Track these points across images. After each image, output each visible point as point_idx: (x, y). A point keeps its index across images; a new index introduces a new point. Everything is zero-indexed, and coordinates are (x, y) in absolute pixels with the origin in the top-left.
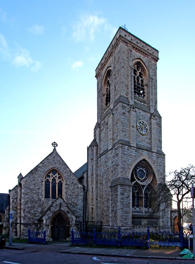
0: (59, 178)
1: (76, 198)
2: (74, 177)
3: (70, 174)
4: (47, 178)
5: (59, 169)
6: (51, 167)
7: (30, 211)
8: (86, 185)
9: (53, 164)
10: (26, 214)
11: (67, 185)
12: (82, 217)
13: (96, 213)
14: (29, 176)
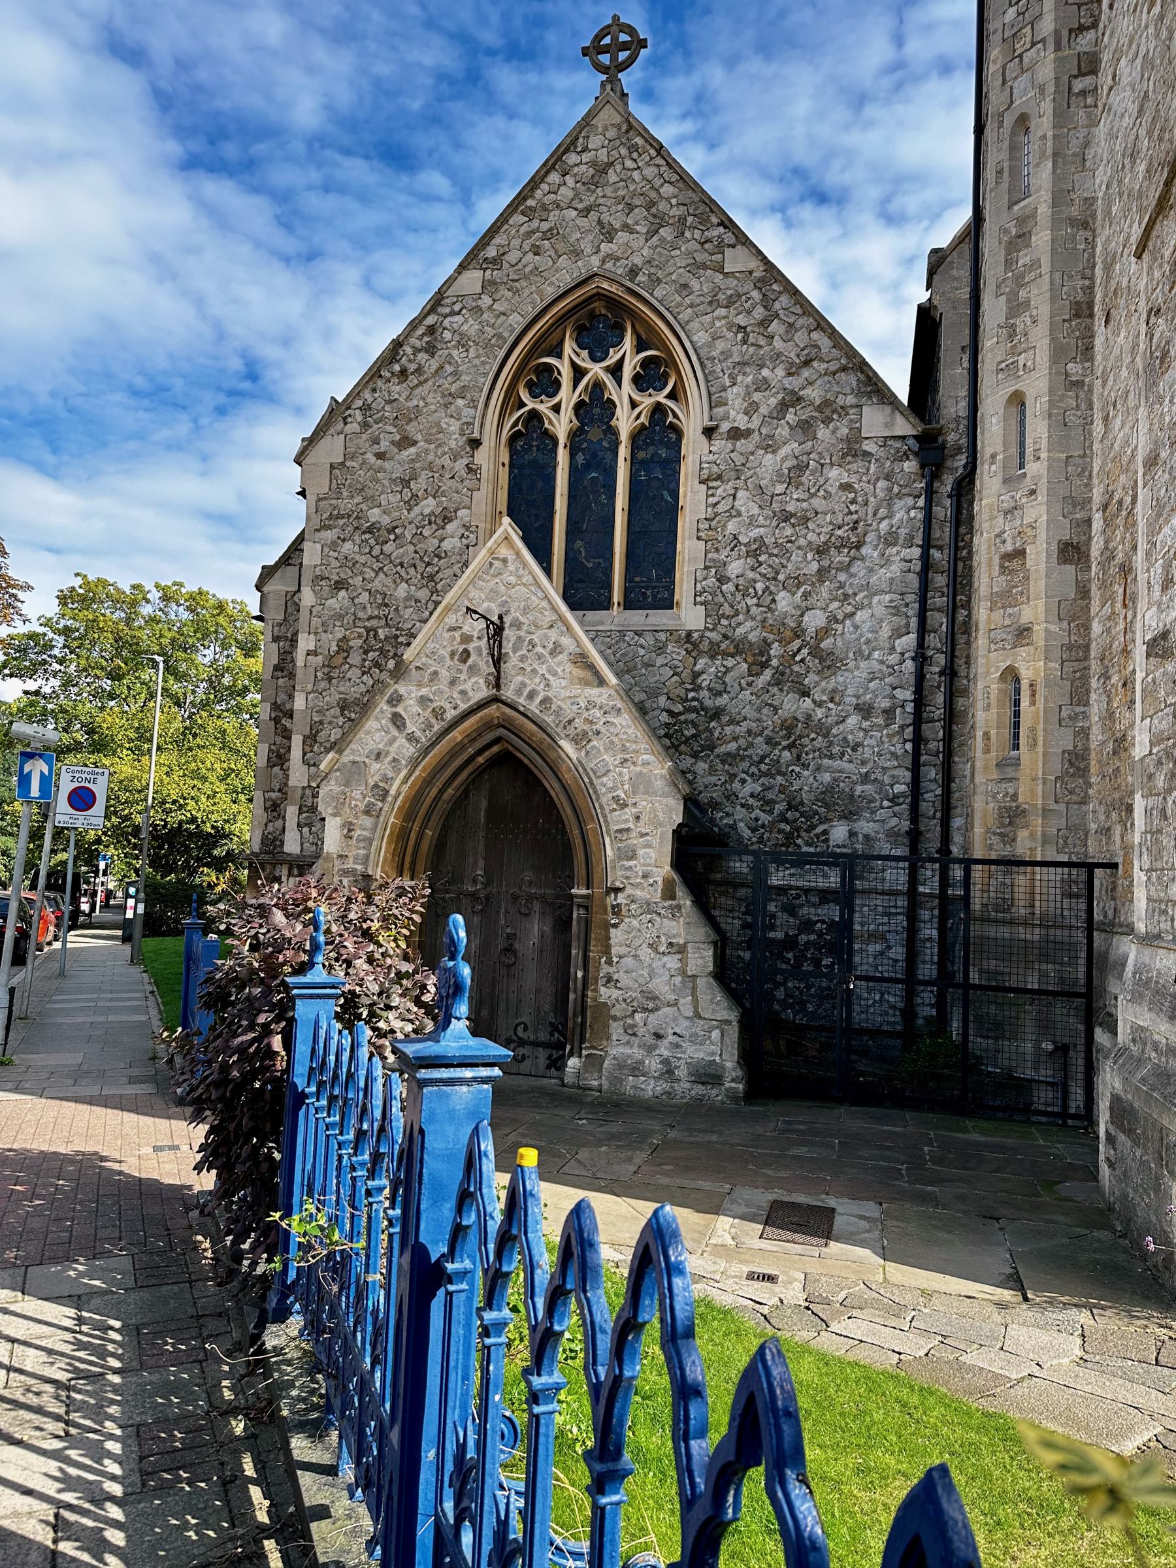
1: (822, 573)
2: (801, 337)
3: (759, 313)
4: (530, 404)
5: (641, 278)
9: (587, 247)
11: (718, 444)
12: (894, 800)
13: (1066, 741)
14: (366, 408)
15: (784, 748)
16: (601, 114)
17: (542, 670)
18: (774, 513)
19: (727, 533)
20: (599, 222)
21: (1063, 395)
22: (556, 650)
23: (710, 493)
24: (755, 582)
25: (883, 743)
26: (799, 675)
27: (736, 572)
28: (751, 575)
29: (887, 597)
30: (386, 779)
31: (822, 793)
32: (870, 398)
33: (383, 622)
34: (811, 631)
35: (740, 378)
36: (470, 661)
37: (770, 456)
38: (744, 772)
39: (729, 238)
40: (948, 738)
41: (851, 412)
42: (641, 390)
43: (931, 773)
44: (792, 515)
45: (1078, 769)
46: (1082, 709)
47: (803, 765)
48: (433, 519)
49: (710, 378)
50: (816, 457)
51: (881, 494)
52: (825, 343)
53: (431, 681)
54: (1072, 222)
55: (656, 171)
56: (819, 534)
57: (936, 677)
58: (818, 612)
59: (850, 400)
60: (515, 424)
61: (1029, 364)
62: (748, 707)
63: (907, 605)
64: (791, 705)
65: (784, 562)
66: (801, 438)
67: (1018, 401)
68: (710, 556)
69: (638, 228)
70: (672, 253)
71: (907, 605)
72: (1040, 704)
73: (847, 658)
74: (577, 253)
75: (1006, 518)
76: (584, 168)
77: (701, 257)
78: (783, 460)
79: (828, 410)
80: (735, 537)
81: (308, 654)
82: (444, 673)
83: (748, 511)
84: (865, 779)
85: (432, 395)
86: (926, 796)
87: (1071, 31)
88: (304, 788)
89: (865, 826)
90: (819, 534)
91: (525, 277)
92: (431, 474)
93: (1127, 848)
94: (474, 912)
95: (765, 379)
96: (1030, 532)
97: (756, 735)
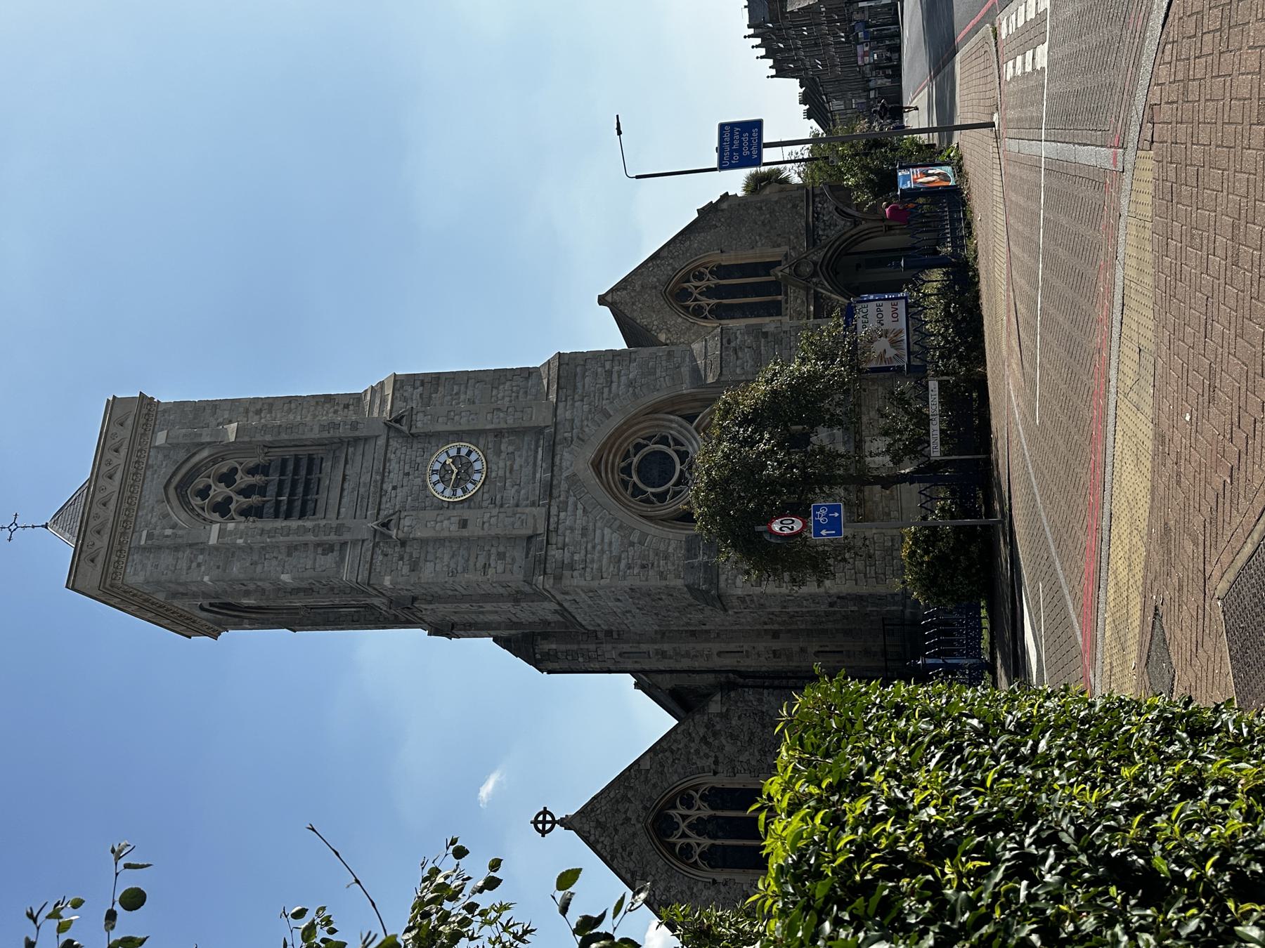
0: (700, 277)
2: (679, 737)
3: (668, 754)
6: (643, 840)
8: (710, 679)
9: (631, 830)
11: (720, 769)
37: (726, 748)
42: (693, 806)
59: (706, 717)
60: (704, 864)
67: (720, 654)
74: (634, 835)
76: (597, 833)
77: (642, 778)
78: (728, 742)
79: (710, 725)
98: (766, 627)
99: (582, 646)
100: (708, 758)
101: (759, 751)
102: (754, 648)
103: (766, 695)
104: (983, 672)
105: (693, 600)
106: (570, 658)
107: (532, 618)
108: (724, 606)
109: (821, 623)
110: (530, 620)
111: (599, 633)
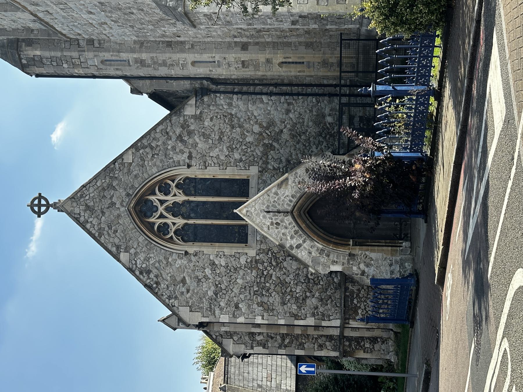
0: (165, 190)
1: (241, 126)
2: (158, 135)
3: (148, 150)
4: (172, 234)
5: (131, 192)
6: (126, 221)
7: (297, 299)
8: (186, 85)
9: (116, 213)
10: (306, 310)
11: (193, 163)
12: (318, 102)
13: (302, 48)
14: (169, 298)
15: (301, 138)
16: (66, 208)
17: (283, 198)
18: (218, 143)
19: (224, 159)
20: (108, 208)
21: (196, 50)
22: (276, 194)
23: (210, 165)
24: (242, 149)
25: (299, 106)
26: (275, 133)
27: (238, 155)
28: (240, 151)
29: (250, 105)
30: (318, 250)
31: (316, 125)
32: (181, 112)
33: (252, 288)
34: (260, 130)
35: (171, 156)
36: (279, 222)
37: (199, 145)
38: (309, 151)
39: (120, 161)
40: (298, 85)
41: (186, 118)
43: (309, 90)
44: (220, 137)
45: (311, 45)
46: (293, 44)
47: (306, 131)
48: (213, 269)
49: (170, 166)
50: (201, 129)
51: (215, 108)
52: (161, 127)
53: (285, 235)
54: (141, 47)
55: (92, 187)
56: (227, 128)
57: (277, 89)
58: (254, 127)
59: (182, 119)
60: (178, 239)
61: (183, 60)
62: (286, 150)
63: (253, 99)
64: (285, 135)
65: (236, 139)
66: (193, 134)
67: (194, 63)
68: (232, 165)
69: (112, 194)
70: (123, 181)
71: (253, 99)
72: (291, 55)
73: (270, 118)
74: (119, 216)
75: (231, 67)
77: (125, 170)
78: (200, 140)
79: (184, 126)
80: (226, 156)
81: (263, 319)
82: (283, 231)
83: (217, 152)
84: (311, 111)
85: (166, 271)
86: (317, 92)
87: (79, 47)
88: (315, 319)
89: (327, 111)
90: (227, 128)
91: (125, 235)
92: (196, 271)
93: (337, 30)
94: (360, 223)
95: (172, 147)
96: (237, 59)
97: (296, 147)
98: (235, 40)
99: (65, 54)
100: (183, 153)
101: (227, 148)
102: (225, 58)
103: (235, 100)
104: (428, 100)
105: (164, 15)
106: (55, 64)
107: (14, 26)
108: (192, 22)
109: (285, 37)
110: (13, 27)
111: (81, 42)
